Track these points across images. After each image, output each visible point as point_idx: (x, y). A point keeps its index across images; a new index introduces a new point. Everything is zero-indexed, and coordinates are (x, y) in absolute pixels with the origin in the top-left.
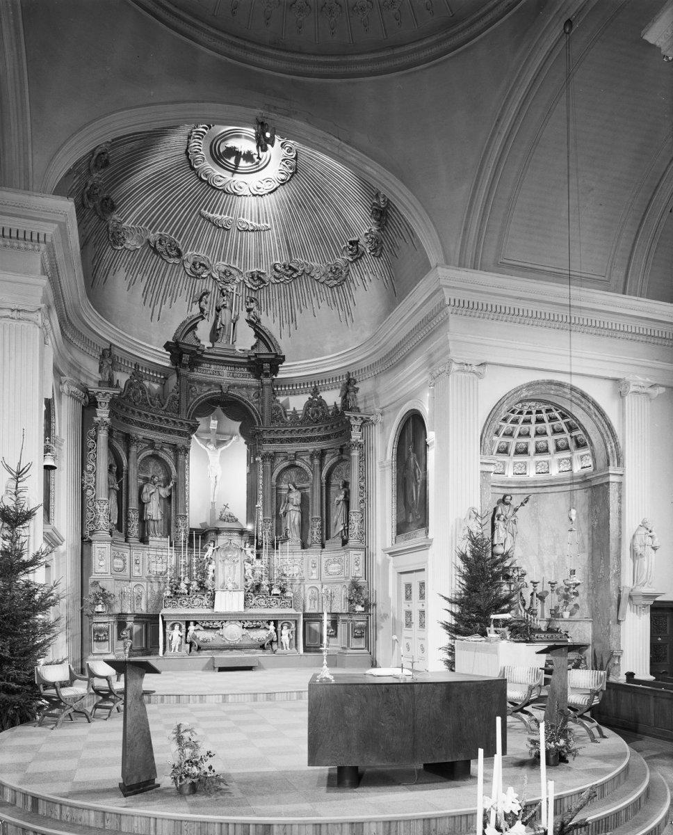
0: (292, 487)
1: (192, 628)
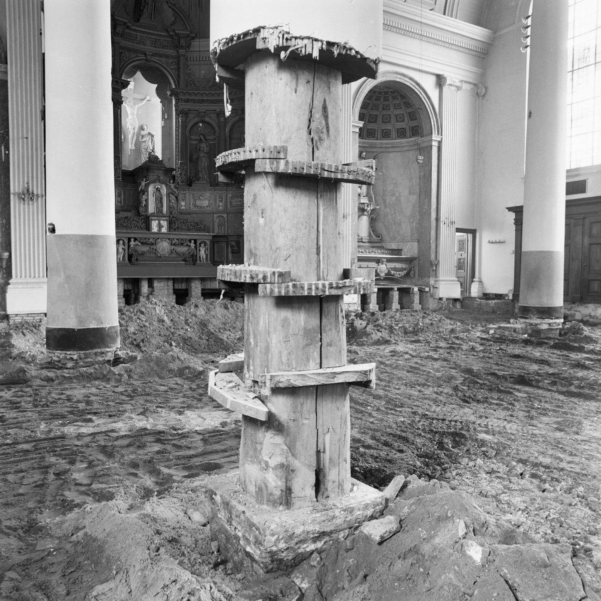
0: (202, 138)
1: (132, 243)
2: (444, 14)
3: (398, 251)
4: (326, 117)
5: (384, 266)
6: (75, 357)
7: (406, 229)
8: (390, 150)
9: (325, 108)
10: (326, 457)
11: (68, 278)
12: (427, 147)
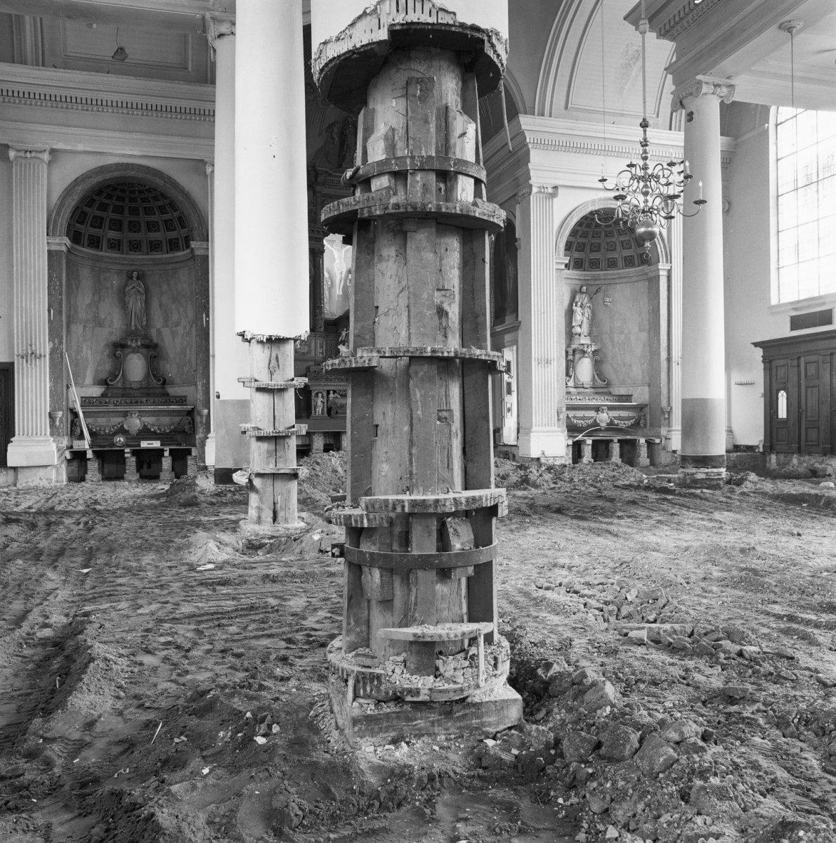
1: (331, 395)
2: (670, 129)
3: (628, 398)
4: (278, 361)
5: (605, 415)
6: (232, 489)
7: (637, 371)
8: (617, 281)
9: (277, 357)
10: (278, 506)
11: (227, 431)
12: (655, 277)
